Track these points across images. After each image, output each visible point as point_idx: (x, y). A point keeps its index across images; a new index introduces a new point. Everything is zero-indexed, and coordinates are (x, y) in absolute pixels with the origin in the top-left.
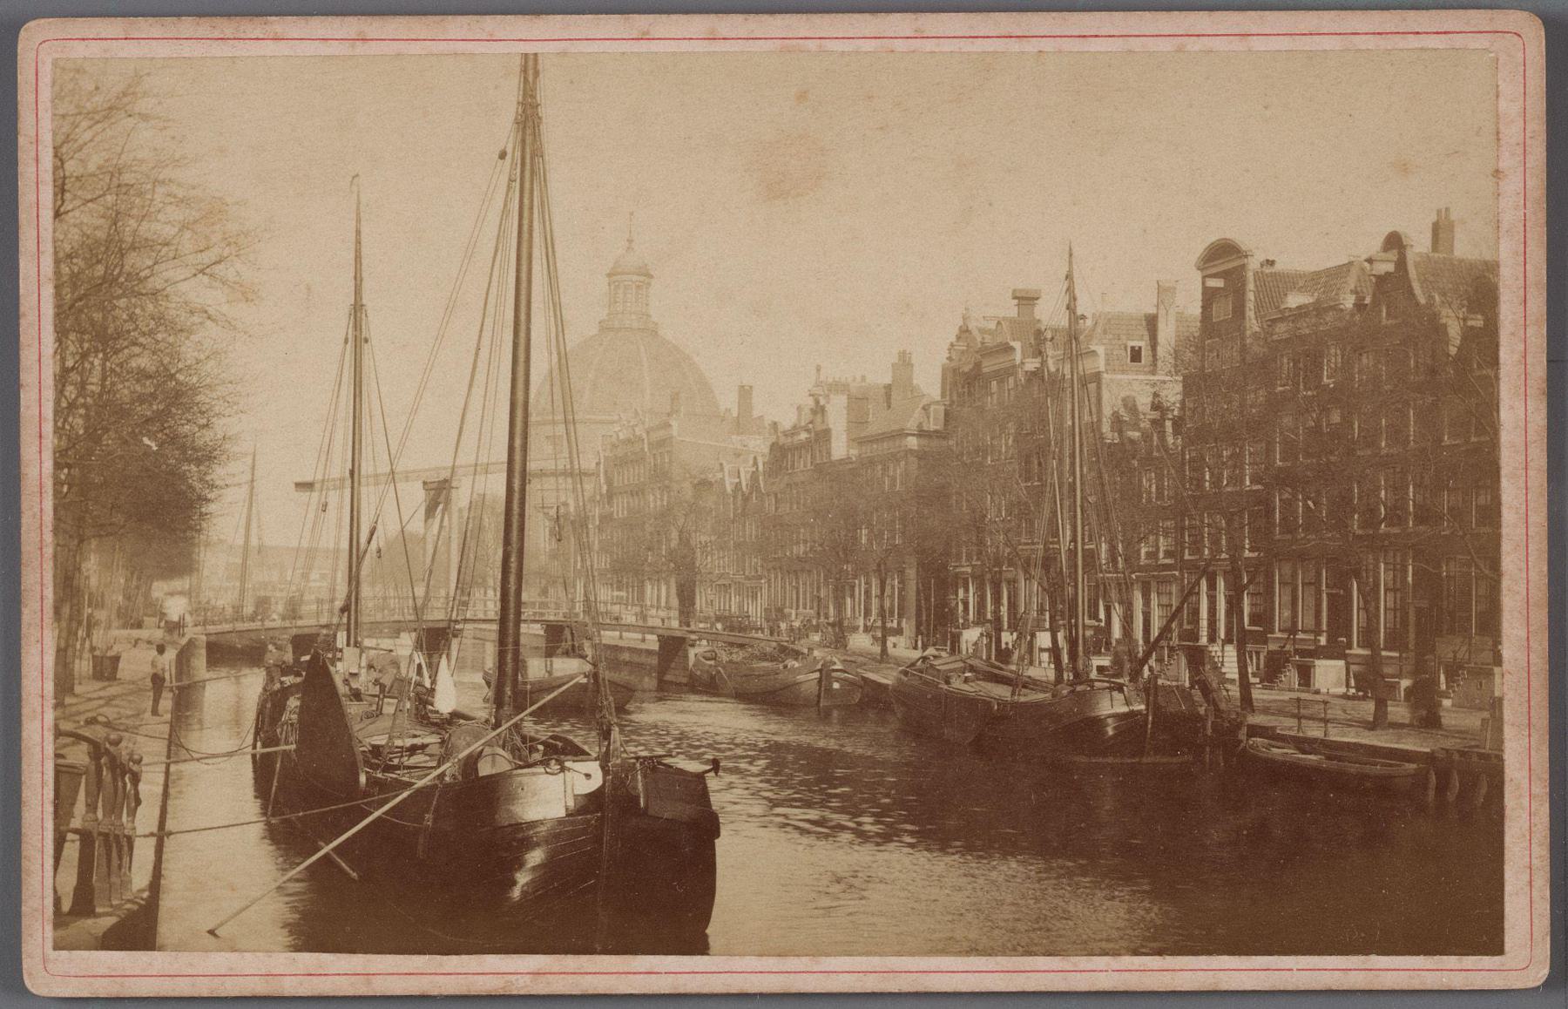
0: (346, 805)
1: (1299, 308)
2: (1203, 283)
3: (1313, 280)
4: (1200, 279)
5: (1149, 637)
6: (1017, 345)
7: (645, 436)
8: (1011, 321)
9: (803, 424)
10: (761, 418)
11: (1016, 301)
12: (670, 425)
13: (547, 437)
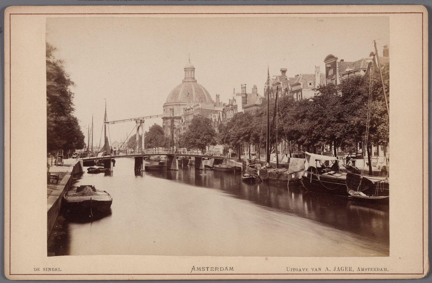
0: (311, 180)
1: (349, 71)
2: (326, 66)
3: (354, 64)
4: (325, 65)
5: (75, 182)
6: (281, 82)
7: (193, 108)
8: (280, 76)
9: (230, 104)
10: (222, 102)
11: (281, 72)
12: (199, 105)
13: (170, 109)
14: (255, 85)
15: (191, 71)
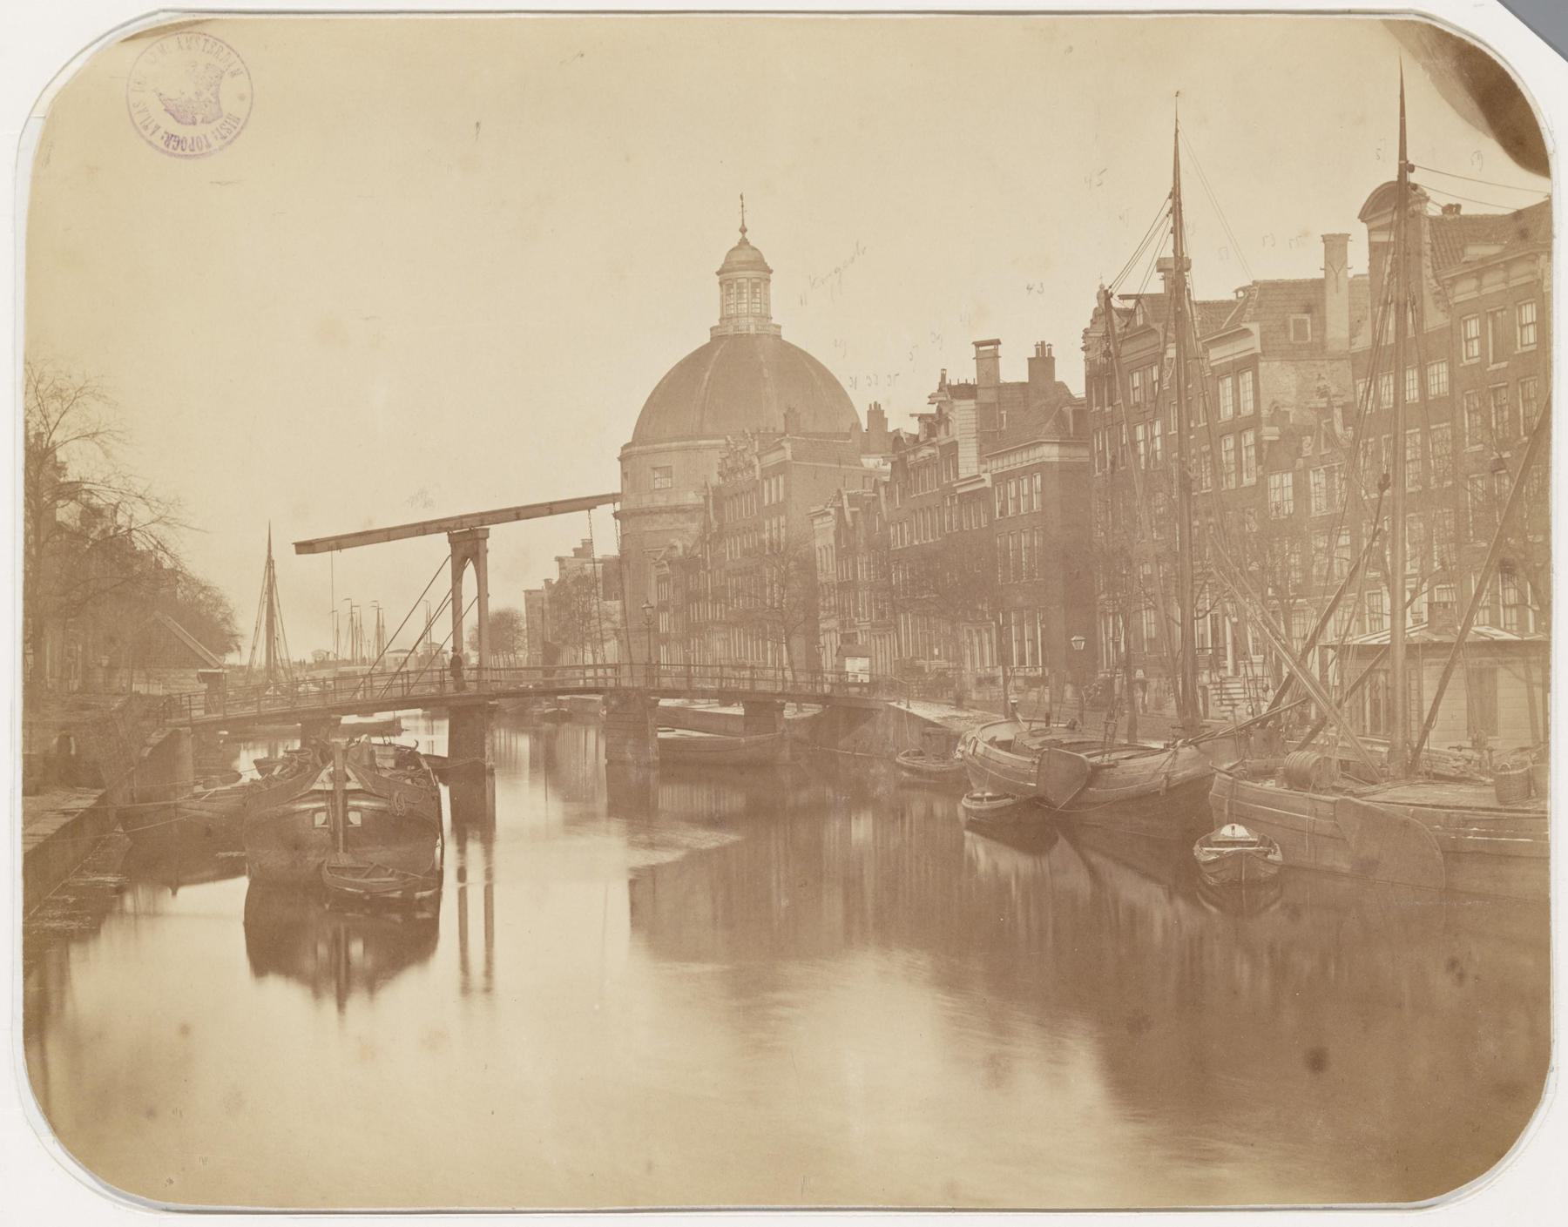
12: (783, 448)
14: (1043, 343)
15: (755, 286)
